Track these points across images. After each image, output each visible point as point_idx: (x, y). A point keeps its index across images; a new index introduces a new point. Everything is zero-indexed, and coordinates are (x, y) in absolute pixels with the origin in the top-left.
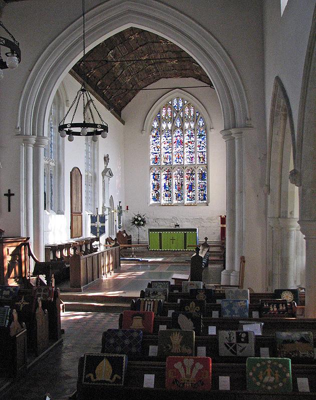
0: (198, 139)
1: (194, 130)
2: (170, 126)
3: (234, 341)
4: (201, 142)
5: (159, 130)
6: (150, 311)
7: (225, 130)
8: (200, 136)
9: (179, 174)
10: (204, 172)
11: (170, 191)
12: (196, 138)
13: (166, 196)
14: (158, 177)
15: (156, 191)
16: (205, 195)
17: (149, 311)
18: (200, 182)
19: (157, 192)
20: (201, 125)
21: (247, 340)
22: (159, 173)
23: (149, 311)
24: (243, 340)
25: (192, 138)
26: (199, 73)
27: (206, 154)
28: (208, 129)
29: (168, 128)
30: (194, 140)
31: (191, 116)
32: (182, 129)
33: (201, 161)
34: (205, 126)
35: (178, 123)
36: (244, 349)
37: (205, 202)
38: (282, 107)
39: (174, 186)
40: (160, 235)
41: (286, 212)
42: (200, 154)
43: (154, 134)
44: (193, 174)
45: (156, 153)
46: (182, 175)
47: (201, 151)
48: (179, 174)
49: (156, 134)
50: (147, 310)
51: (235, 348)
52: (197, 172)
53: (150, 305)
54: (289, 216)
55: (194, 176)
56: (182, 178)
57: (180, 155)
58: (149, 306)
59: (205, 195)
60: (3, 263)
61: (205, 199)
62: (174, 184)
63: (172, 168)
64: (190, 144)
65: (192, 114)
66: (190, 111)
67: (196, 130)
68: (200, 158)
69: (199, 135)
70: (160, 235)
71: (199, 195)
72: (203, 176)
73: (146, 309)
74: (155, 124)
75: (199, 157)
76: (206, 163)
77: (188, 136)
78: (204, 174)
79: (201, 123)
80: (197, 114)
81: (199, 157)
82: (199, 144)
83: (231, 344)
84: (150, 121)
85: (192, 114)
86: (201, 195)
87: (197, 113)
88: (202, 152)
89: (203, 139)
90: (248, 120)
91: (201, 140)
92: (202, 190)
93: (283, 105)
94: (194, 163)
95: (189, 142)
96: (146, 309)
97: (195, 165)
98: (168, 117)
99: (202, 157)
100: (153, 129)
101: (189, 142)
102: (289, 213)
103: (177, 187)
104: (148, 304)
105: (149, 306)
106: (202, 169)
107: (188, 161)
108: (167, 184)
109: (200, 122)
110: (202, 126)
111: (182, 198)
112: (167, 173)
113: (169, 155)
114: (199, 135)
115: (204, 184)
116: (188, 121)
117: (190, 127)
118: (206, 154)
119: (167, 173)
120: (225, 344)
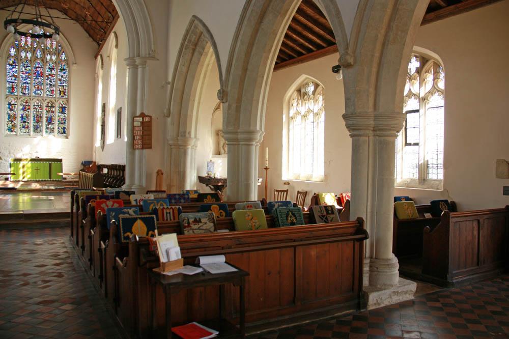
0: (59, 73)
1: (56, 63)
2: (29, 55)
3: (325, 213)
4: (62, 76)
5: (17, 56)
6: (171, 220)
7: (129, 58)
8: (62, 70)
9: (38, 106)
10: (64, 105)
11: (28, 123)
12: (57, 72)
13: (24, 127)
14: (15, 107)
15: (12, 121)
16: (64, 128)
17: (169, 219)
18: (60, 115)
19: (13, 123)
20: (63, 59)
21: (333, 213)
22: (16, 103)
23: (169, 219)
24: (330, 212)
25: (53, 71)
26: (66, 7)
27: (67, 88)
28: (70, 63)
29: (27, 58)
30: (55, 73)
31: (53, 49)
32: (43, 60)
33: (62, 95)
34: (66, 61)
35: (39, 54)
36: (332, 219)
37: (65, 135)
38: (193, 43)
39: (32, 118)
40: (50, 165)
41: (185, 132)
42: (61, 87)
43: (11, 62)
44: (53, 107)
45: (12, 82)
46: (41, 107)
47: (62, 85)
48: (38, 106)
49: (14, 62)
50: (167, 220)
51: (326, 219)
52: (57, 105)
53: (170, 213)
54: (187, 135)
55: (54, 109)
56: (41, 110)
57: (40, 87)
58: (168, 215)
59: (64, 128)
60: (446, 78)
61: (64, 132)
62: (32, 115)
63: (30, 99)
64: (50, 77)
65: (54, 47)
66: (52, 44)
67: (57, 63)
68: (60, 91)
69: (60, 69)
70: (50, 165)
71: (59, 128)
72: (63, 109)
73: (165, 219)
74: (13, 51)
75: (59, 90)
76: (67, 97)
77: (49, 68)
78: (65, 108)
79: (63, 57)
80: (60, 48)
81: (59, 90)
82: (61, 78)
83: (324, 216)
84: (8, 45)
85: (54, 47)
86: (60, 128)
87: (60, 46)
88: (63, 86)
89: (65, 73)
90: (152, 51)
91: (62, 74)
92: (62, 123)
93: (194, 40)
94: (54, 96)
95: (50, 75)
96: (165, 219)
97: (55, 98)
98: (28, 47)
99: (63, 91)
100: (9, 56)
101: (50, 75)
102: (187, 133)
103: (36, 119)
104: (167, 213)
105: (168, 215)
106: (62, 103)
107: (48, 93)
108: (24, 115)
109: (62, 56)
110: (64, 61)
111: (41, 130)
112: (24, 104)
113: (28, 85)
114: (60, 69)
115: (64, 117)
116: (50, 53)
117: (51, 59)
118: (67, 88)
119: (24, 104)
120: (319, 216)
